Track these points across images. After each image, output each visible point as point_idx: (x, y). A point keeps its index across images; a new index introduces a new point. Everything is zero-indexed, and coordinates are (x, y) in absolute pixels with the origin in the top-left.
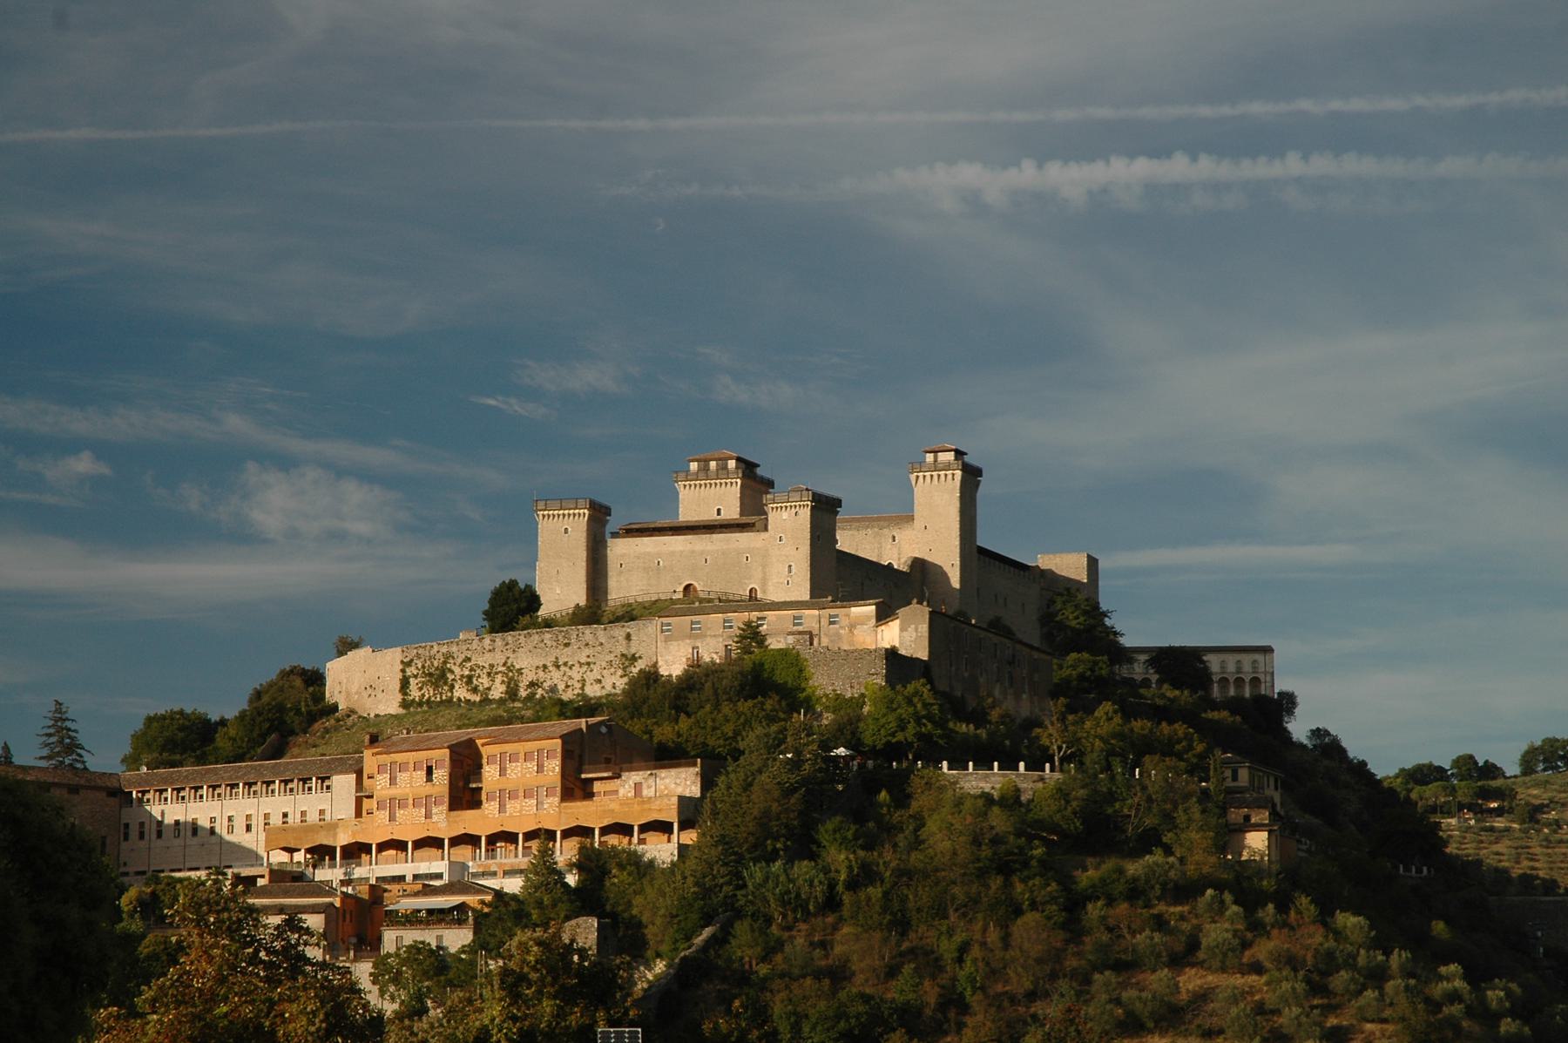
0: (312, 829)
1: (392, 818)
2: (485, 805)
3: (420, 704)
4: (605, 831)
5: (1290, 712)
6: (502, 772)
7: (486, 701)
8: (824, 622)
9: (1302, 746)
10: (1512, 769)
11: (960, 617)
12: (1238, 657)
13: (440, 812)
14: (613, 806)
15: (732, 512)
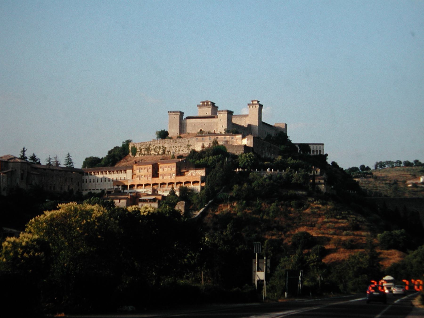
2: (160, 177)
3: (144, 155)
4: (185, 183)
7: (158, 154)
8: (231, 139)
9: (329, 165)
10: (372, 168)
11: (258, 138)
12: (316, 146)
13: (150, 178)
15: (209, 114)
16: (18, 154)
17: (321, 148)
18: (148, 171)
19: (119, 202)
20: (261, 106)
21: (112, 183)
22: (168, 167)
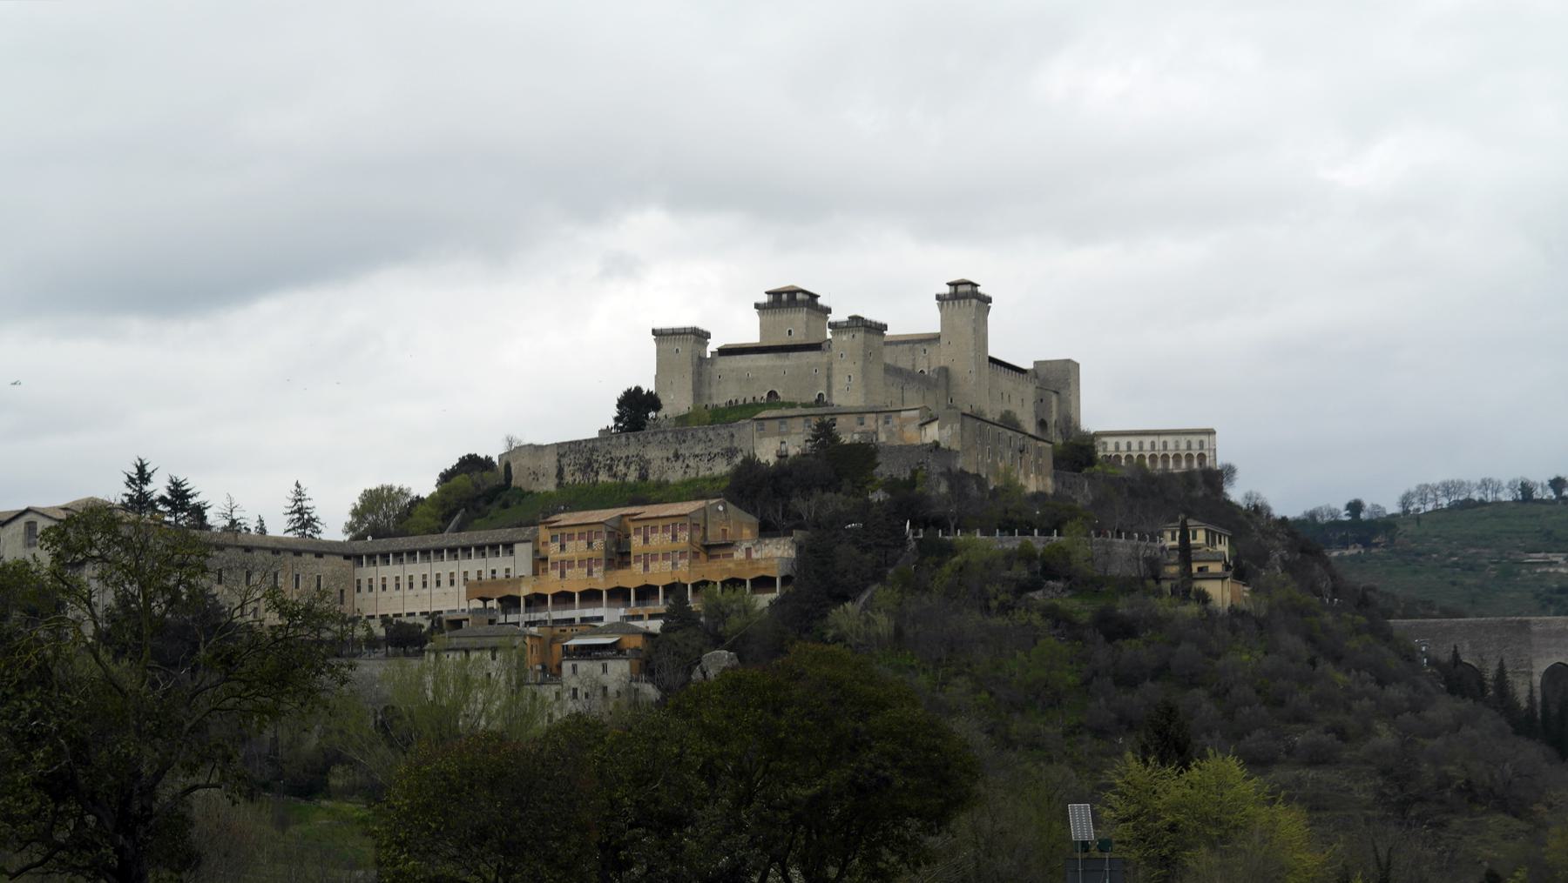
0: (500, 584)
1: (563, 575)
5: (1230, 481)
6: (646, 540)
7: (624, 484)
12: (1189, 437)
13: (598, 572)
14: (731, 565)
16: (114, 491)
17: (1206, 446)
21: (464, 589)
22: (581, 536)
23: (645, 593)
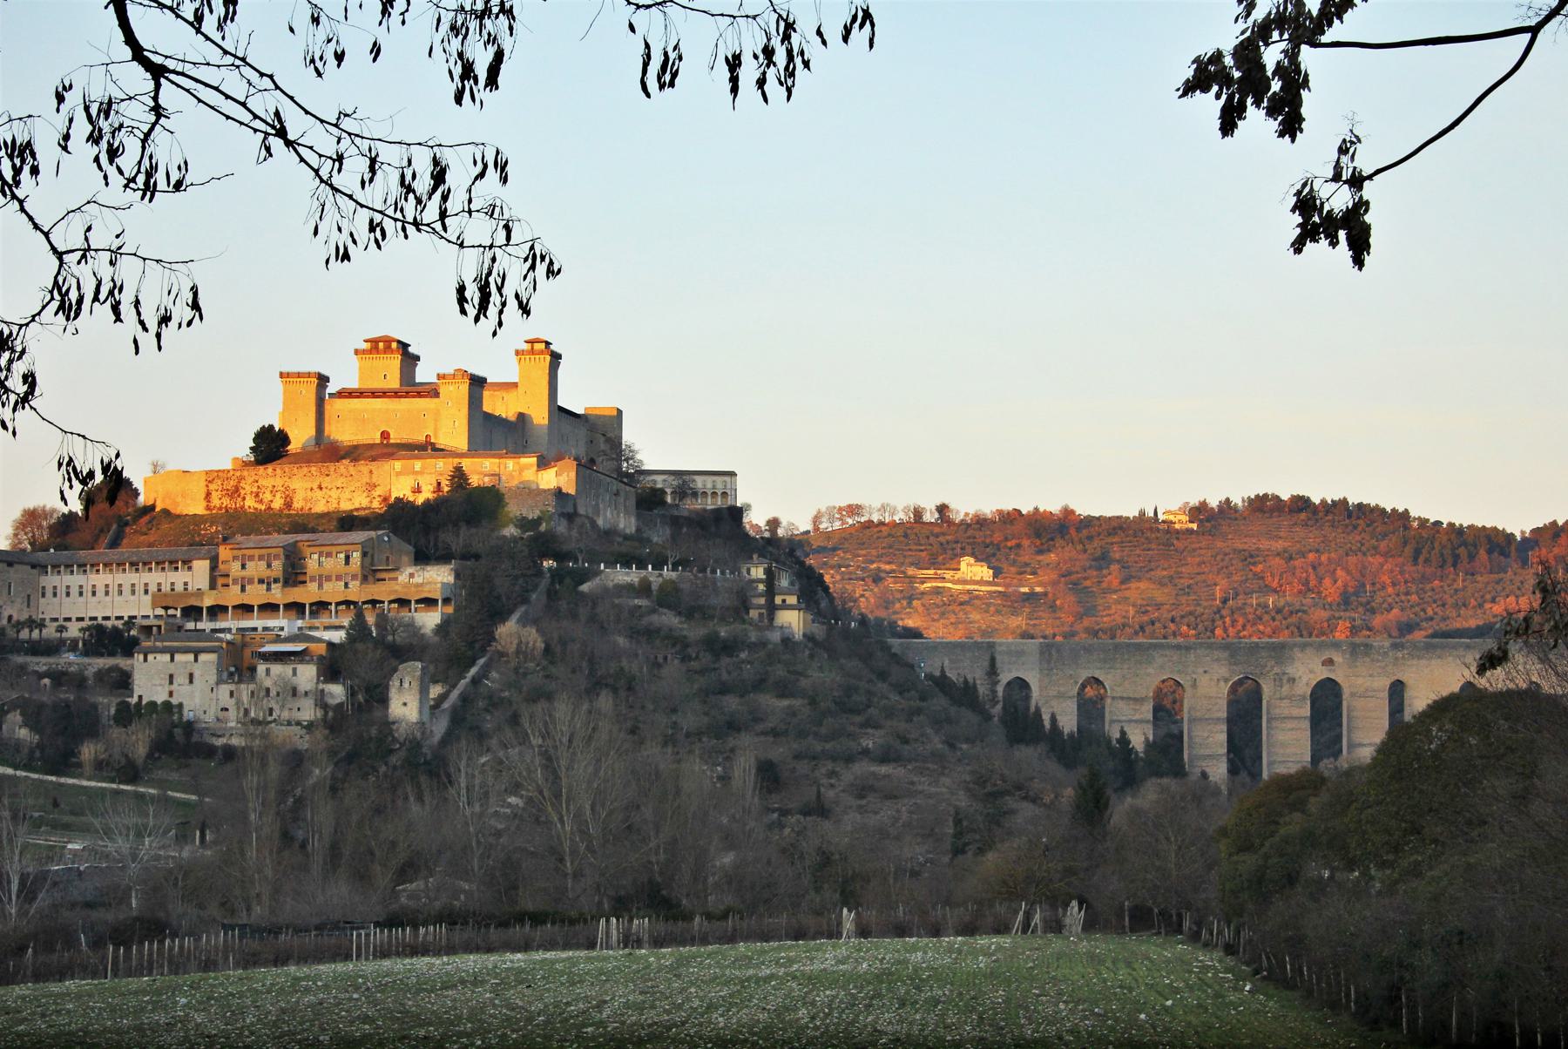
0: (180, 595)
18: (269, 566)
19: (196, 660)
20: (556, 357)
22: (261, 558)
23: (321, 606)
